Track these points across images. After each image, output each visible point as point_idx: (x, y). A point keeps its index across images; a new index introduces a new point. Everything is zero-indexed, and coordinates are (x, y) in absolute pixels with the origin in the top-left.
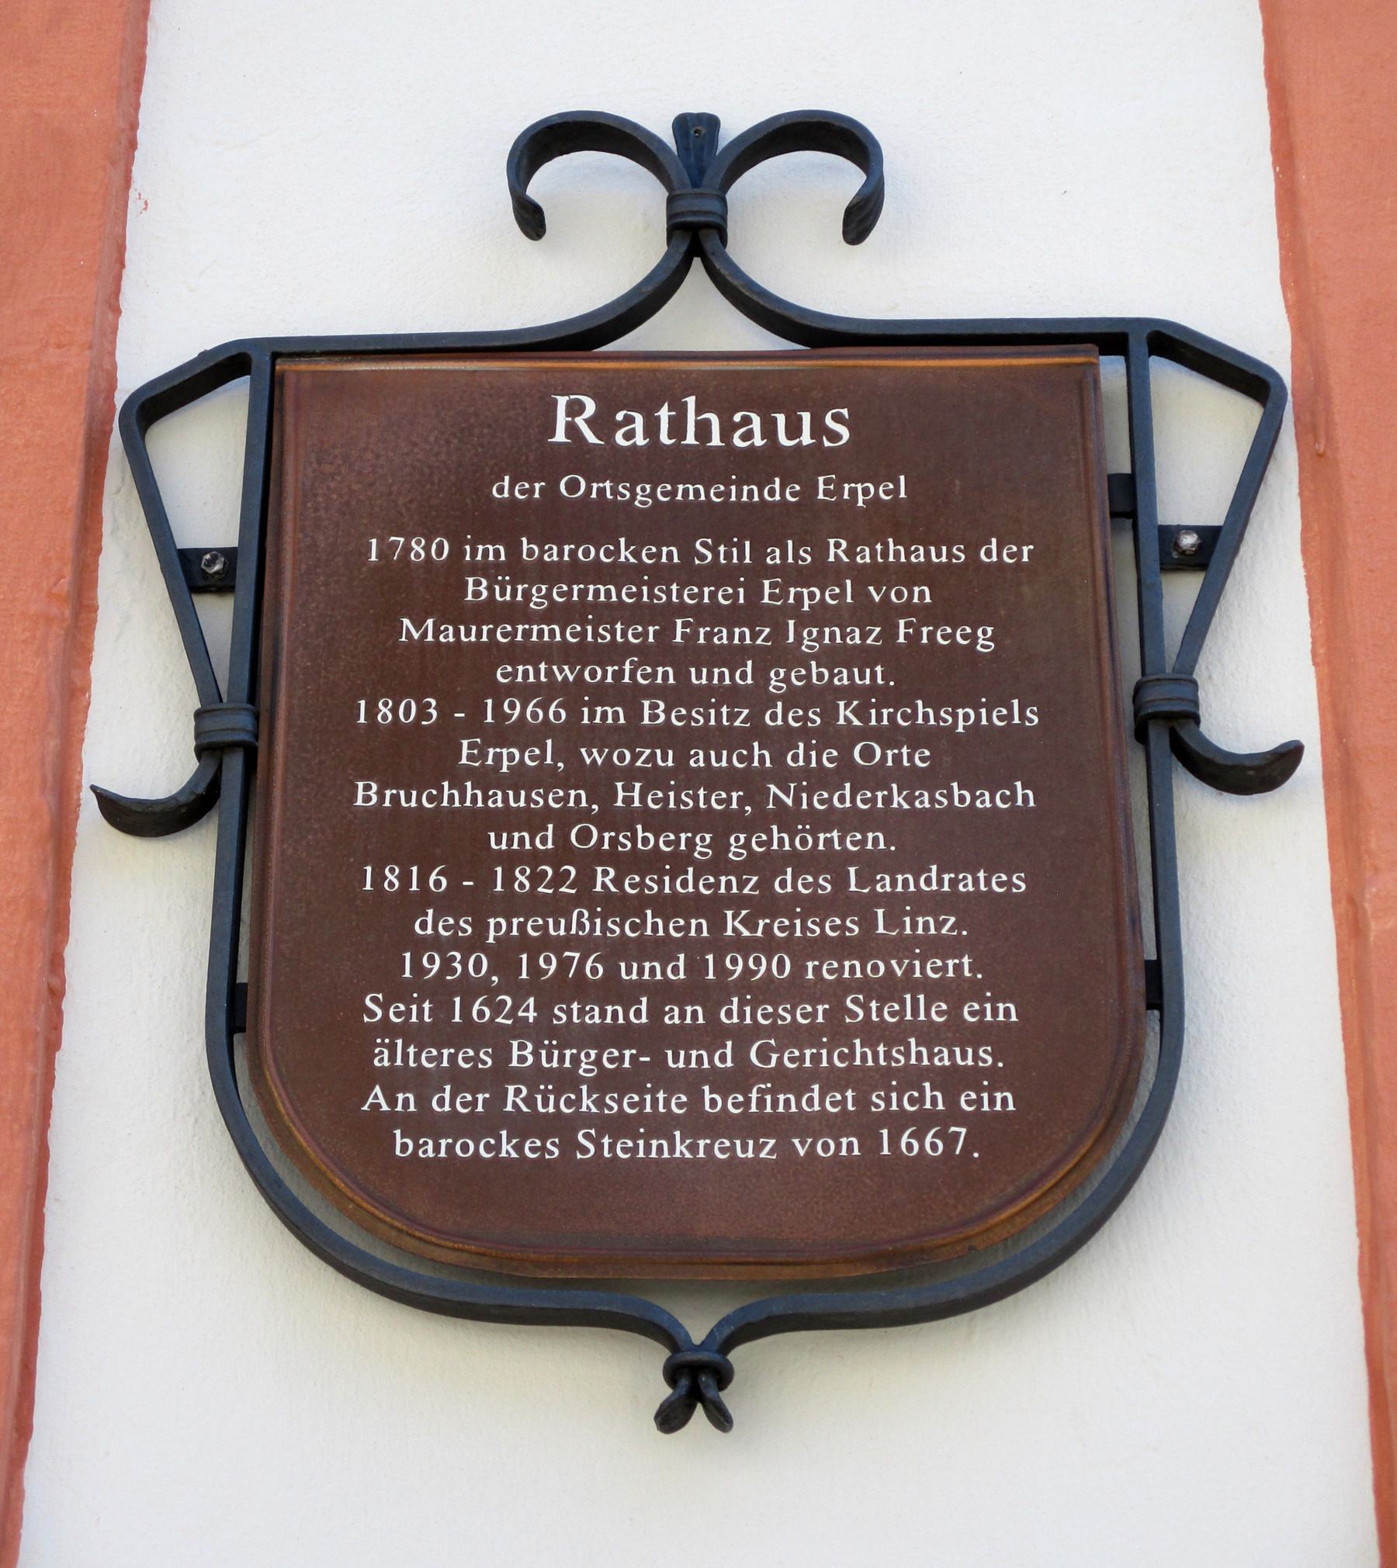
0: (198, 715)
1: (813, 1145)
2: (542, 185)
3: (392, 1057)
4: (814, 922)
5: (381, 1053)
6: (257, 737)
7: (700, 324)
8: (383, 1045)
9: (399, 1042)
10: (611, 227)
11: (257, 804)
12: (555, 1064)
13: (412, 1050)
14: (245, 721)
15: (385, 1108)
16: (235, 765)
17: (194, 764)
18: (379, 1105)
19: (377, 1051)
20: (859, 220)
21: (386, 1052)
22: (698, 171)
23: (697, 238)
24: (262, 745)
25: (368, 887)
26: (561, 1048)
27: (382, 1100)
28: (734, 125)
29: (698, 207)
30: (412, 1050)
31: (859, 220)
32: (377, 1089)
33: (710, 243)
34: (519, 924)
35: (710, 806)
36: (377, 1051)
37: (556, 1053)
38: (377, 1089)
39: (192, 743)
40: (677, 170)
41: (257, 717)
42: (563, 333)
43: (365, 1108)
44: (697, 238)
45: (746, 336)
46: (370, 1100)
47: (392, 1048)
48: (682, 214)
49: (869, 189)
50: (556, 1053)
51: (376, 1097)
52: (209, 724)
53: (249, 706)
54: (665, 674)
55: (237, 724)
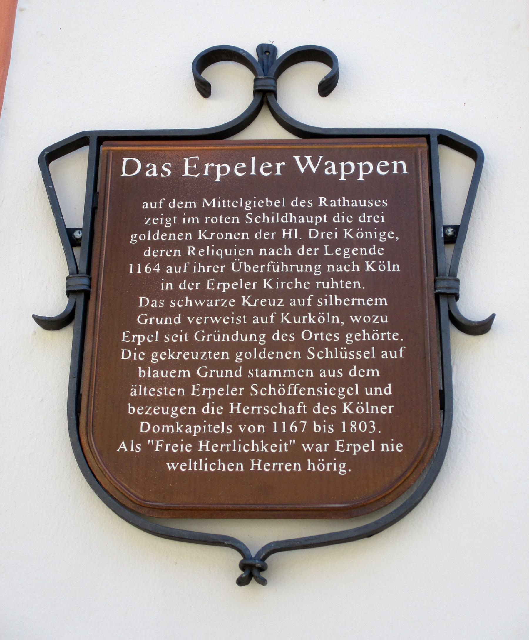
0: (68, 278)
1: (362, 318)
2: (208, 74)
3: (138, 392)
4: (370, 201)
5: (133, 390)
6: (90, 286)
7: (266, 129)
8: (134, 387)
9: (140, 386)
10: (234, 92)
11: (99, 212)
12: (219, 340)
13: (145, 389)
14: (86, 281)
15: (126, 450)
16: (81, 299)
17: (67, 299)
18: (124, 449)
19: (132, 390)
20: (326, 87)
21: (135, 390)
22: (269, 67)
23: (265, 98)
24: (93, 291)
25: (139, 272)
26: (221, 334)
27: (125, 447)
28: (282, 51)
29: (267, 84)
30: (145, 389)
31: (326, 87)
32: (123, 443)
33: (270, 98)
34: (210, 268)
35: (213, 432)
36: (132, 390)
37: (219, 335)
38: (123, 443)
39: (65, 289)
40: (259, 69)
41: (90, 279)
42: (213, 132)
43: (118, 450)
44: (265, 98)
45: (281, 134)
46: (120, 447)
47: (138, 389)
48: (259, 86)
49: (332, 74)
50: (219, 335)
51: (122, 446)
52: (74, 282)
53: (87, 275)
54: (249, 252)
55: (82, 283)
